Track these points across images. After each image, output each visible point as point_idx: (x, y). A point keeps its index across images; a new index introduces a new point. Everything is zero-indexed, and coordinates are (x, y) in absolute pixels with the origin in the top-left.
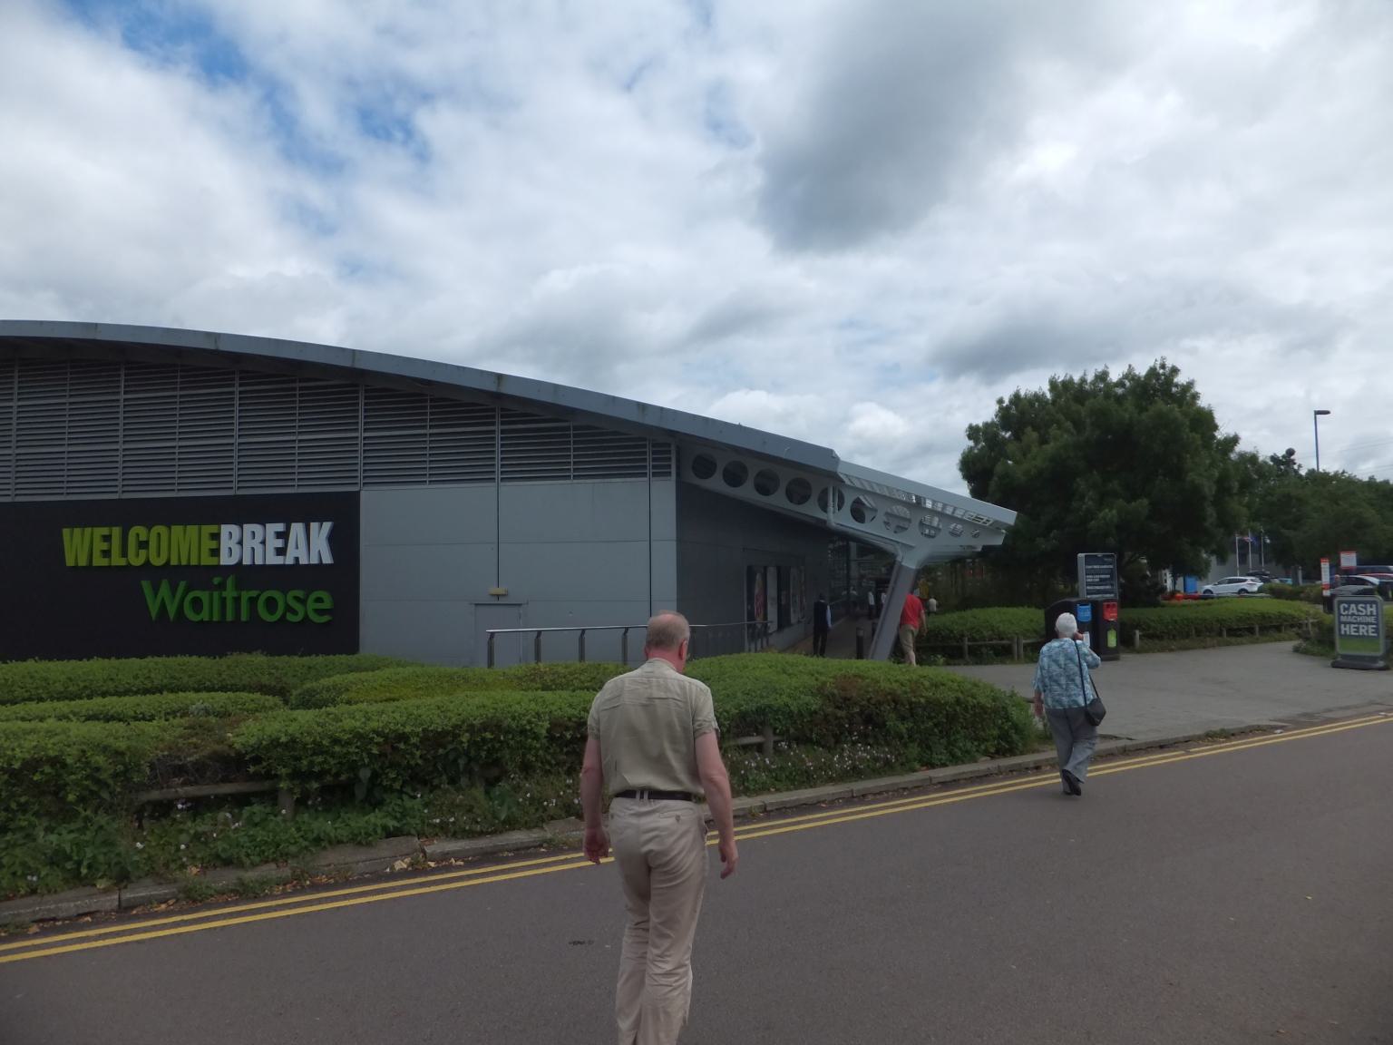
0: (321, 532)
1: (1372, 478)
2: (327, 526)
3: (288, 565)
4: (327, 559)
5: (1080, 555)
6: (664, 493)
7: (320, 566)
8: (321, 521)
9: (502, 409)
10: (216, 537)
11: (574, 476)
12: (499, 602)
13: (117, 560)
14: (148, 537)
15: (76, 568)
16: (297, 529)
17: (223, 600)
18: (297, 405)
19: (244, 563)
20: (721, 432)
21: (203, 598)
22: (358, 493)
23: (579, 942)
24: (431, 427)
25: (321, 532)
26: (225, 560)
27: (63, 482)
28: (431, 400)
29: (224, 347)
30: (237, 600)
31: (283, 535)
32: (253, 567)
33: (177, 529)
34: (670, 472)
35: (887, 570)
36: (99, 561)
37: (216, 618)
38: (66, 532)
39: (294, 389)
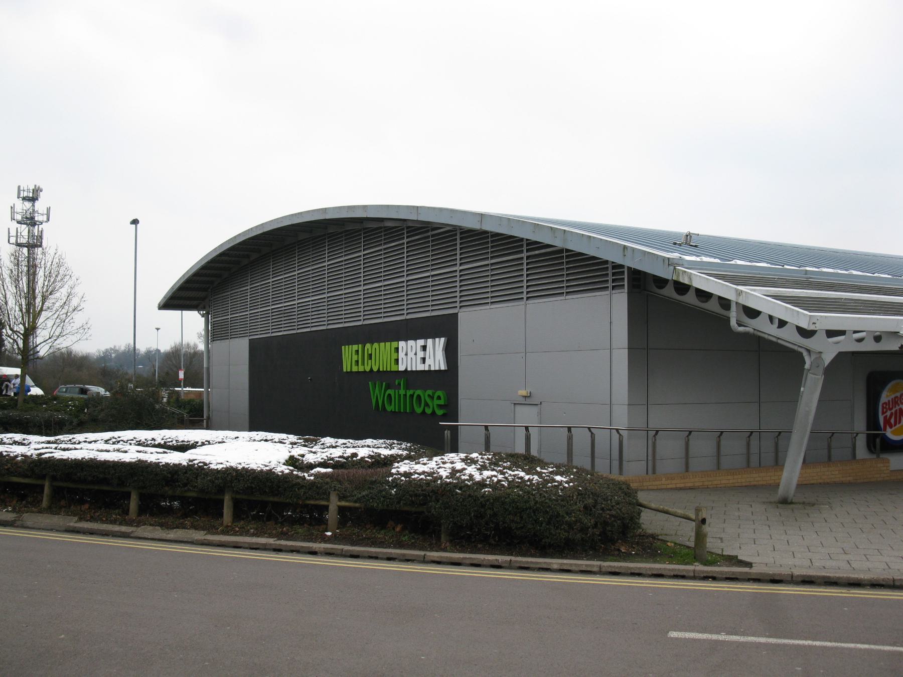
0: (441, 342)
1: (82, 459)
2: (443, 339)
3: (426, 371)
4: (443, 368)
5: (348, 365)
6: (620, 301)
7: (440, 371)
8: (440, 337)
9: (408, 228)
10: (397, 349)
11: (566, 292)
12: (526, 403)
13: (361, 369)
14: (358, 348)
15: (347, 372)
16: (430, 341)
17: (400, 395)
18: (564, 261)
19: (408, 370)
20: (436, 215)
21: (391, 393)
22: (456, 315)
23: (822, 545)
24: (492, 258)
25: (441, 342)
26: (402, 368)
27: (342, 314)
28: (385, 231)
29: (488, 227)
30: (405, 395)
31: (424, 348)
32: (412, 371)
33: (382, 344)
34: (624, 285)
35: (254, 533)
36: (355, 369)
37: (397, 410)
38: (343, 347)
39: (428, 237)
